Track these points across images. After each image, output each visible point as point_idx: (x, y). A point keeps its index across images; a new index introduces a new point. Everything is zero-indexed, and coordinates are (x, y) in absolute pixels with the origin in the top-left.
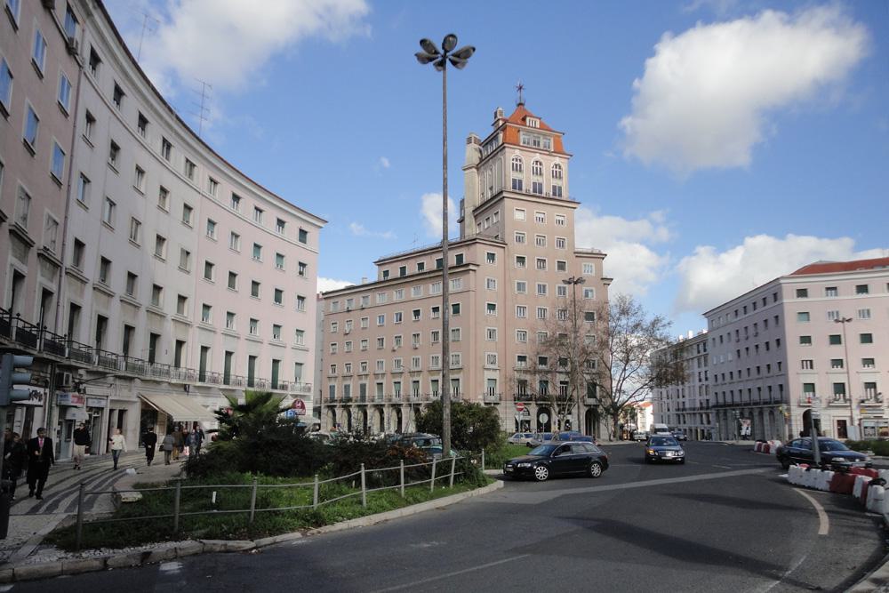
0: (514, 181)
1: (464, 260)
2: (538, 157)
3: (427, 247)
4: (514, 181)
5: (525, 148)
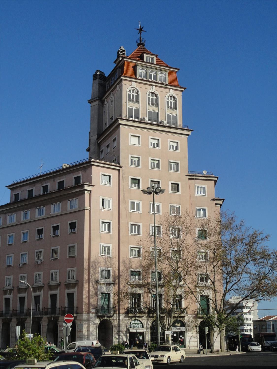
0: (130, 110)
1: (65, 186)
2: (154, 89)
3: (52, 171)
4: (130, 110)
5: (146, 81)
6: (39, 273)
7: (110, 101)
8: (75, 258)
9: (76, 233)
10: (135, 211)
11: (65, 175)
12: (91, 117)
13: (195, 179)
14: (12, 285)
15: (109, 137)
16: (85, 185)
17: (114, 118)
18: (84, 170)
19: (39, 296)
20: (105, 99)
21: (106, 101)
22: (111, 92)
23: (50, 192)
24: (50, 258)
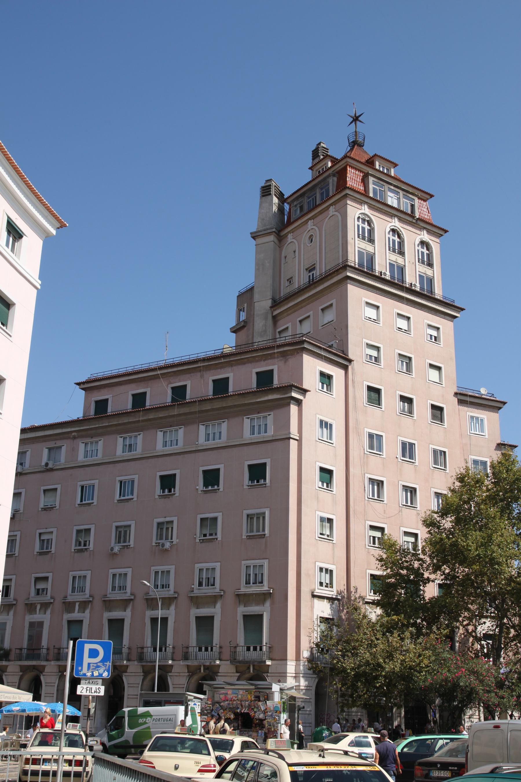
3: (202, 356)
6: (165, 568)
7: (305, 237)
8: (264, 540)
9: (265, 487)
10: (375, 452)
11: (232, 366)
12: (257, 264)
13: (470, 402)
14: (87, 591)
15: (308, 304)
16: (293, 388)
17: (320, 269)
18: (281, 358)
19: (122, 621)
20: (289, 232)
21: (290, 236)
22: (310, 219)
23: (150, 406)
24: (195, 538)
